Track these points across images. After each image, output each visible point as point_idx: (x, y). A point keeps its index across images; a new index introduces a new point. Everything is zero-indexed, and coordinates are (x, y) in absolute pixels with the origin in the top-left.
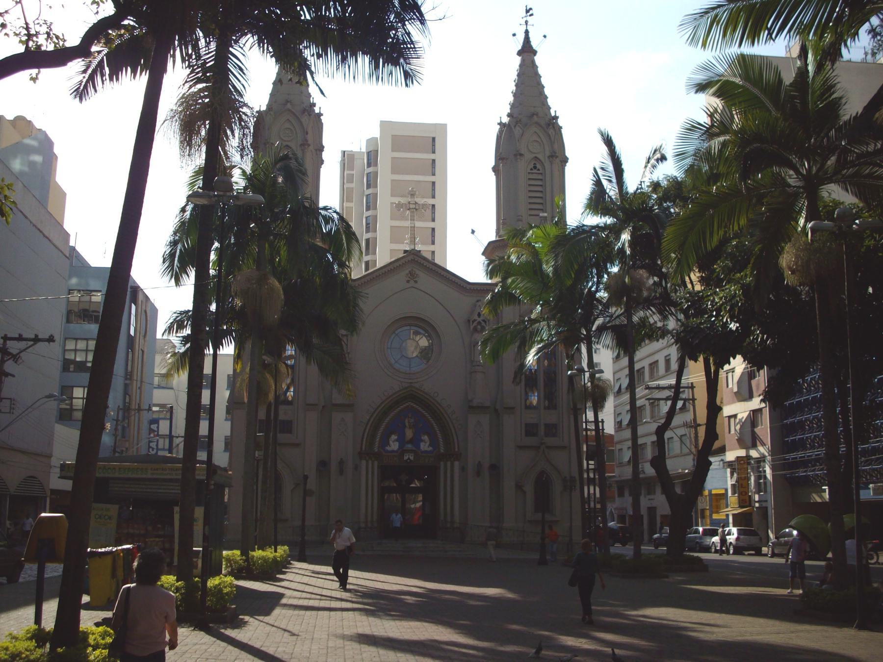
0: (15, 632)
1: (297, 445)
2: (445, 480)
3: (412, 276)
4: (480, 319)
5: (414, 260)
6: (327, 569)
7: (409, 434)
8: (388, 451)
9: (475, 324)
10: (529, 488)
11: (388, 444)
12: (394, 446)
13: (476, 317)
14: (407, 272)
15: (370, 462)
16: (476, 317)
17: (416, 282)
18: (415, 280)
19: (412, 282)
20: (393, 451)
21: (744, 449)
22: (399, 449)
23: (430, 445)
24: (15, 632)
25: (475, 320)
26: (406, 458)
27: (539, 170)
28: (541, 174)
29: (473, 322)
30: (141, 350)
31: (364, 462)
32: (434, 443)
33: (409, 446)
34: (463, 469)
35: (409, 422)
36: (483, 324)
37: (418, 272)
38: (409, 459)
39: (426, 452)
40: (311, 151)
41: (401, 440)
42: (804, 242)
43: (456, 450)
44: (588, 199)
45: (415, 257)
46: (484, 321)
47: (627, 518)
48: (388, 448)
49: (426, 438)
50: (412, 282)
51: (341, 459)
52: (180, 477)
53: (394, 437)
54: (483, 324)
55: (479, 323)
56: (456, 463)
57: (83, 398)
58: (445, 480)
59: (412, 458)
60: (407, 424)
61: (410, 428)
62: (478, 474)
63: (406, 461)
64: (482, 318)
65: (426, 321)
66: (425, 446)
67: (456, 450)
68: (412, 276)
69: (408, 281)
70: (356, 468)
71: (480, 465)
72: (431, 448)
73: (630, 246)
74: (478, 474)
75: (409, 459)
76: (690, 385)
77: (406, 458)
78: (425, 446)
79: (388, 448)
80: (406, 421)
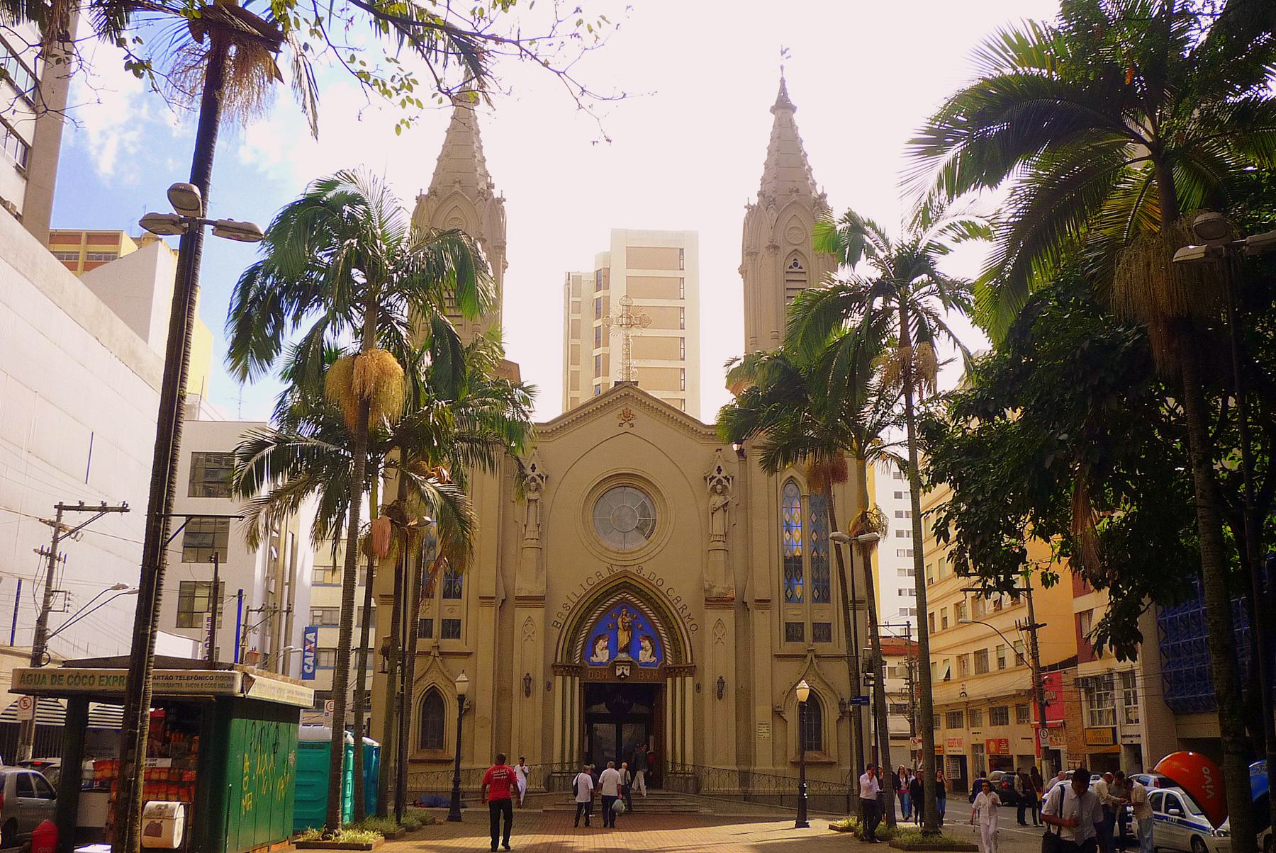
19: (626, 425)
50: (626, 425)
69: (621, 425)
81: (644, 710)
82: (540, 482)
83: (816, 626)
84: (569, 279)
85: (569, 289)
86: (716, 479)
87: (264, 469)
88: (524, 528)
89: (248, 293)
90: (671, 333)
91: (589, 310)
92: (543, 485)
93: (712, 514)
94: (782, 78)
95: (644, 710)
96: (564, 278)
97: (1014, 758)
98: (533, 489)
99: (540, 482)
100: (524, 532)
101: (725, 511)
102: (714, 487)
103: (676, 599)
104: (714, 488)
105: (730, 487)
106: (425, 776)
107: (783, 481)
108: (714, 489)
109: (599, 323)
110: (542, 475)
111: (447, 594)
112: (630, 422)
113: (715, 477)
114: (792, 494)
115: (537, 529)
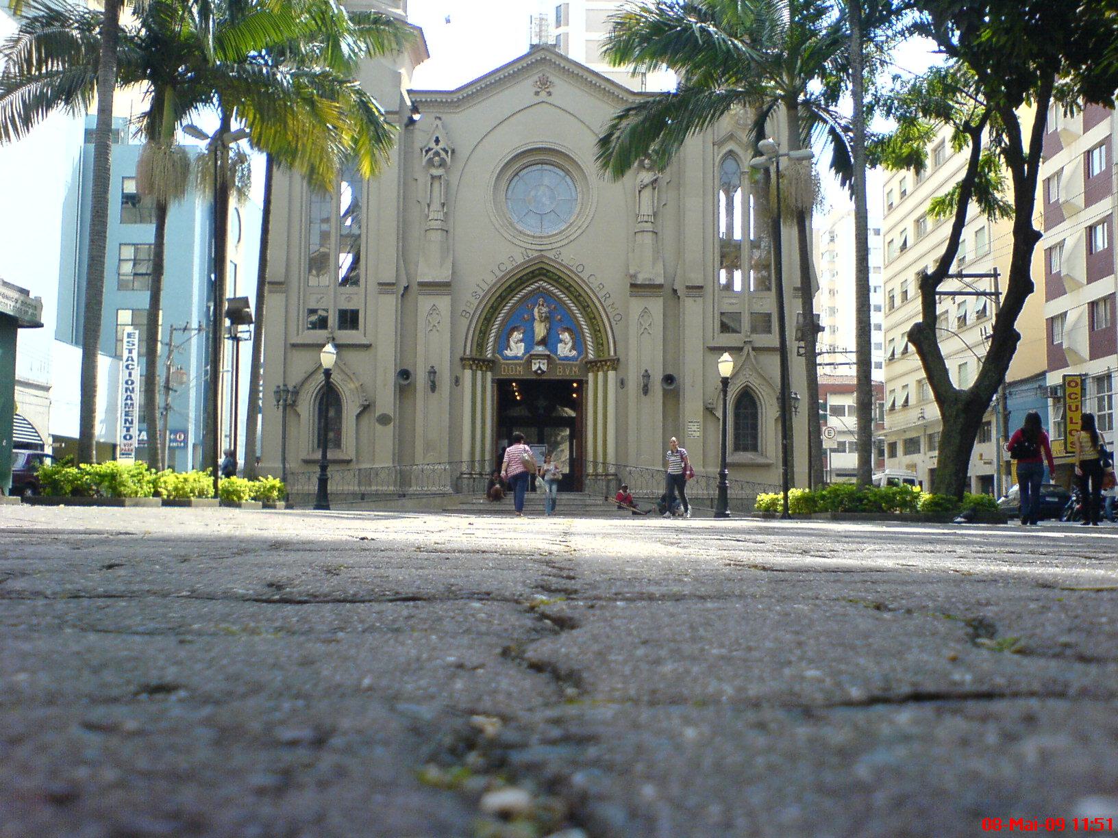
0: (474, 658)
1: (367, 347)
2: (483, 400)
3: (544, 84)
4: (438, 148)
5: (545, 59)
7: (540, 330)
8: (508, 358)
9: (431, 154)
10: (307, 407)
11: (508, 346)
12: (517, 348)
13: (432, 145)
14: (536, 78)
15: (479, 373)
16: (432, 145)
17: (549, 94)
18: (547, 90)
19: (543, 94)
20: (516, 358)
21: (16, 332)
22: (524, 354)
23: (573, 348)
24: (474, 658)
25: (430, 149)
26: (534, 368)
29: (427, 152)
31: (468, 373)
32: (578, 344)
33: (540, 349)
34: (622, 383)
35: (539, 312)
37: (552, 78)
38: (540, 368)
39: (566, 358)
41: (529, 341)
43: (612, 353)
45: (546, 53)
46: (444, 150)
47: (847, 446)
48: (508, 353)
49: (566, 336)
50: (543, 94)
51: (646, 371)
53: (517, 336)
55: (437, 154)
56: (611, 374)
57: (149, 260)
58: (483, 400)
59: (544, 368)
60: (537, 316)
61: (542, 322)
62: (646, 390)
63: (536, 372)
64: (442, 145)
65: (567, 156)
66: (565, 349)
67: (612, 353)
68: (544, 84)
69: (537, 93)
70: (457, 381)
71: (647, 376)
72: (574, 353)
73: (632, 55)
74: (646, 390)
75: (540, 368)
76: (992, 272)
77: (534, 368)
78: (565, 349)
79: (508, 353)
80: (536, 310)
81: (571, 413)
82: (445, 156)
92: (448, 160)
93: (640, 192)
99: (445, 156)
101: (654, 189)
107: (721, 155)
112: (547, 90)
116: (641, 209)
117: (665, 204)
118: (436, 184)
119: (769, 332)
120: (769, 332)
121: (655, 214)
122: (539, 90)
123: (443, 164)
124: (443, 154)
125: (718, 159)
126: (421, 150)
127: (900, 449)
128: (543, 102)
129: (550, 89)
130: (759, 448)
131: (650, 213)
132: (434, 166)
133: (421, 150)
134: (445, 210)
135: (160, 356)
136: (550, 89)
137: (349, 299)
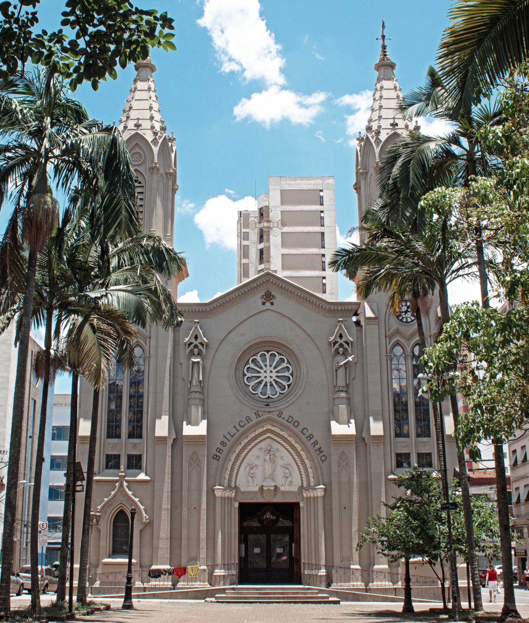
3: (268, 297)
4: (341, 341)
6: (355, 538)
9: (337, 345)
17: (272, 304)
18: (271, 301)
19: (268, 304)
27: (140, 183)
28: (143, 187)
29: (189, 345)
30: (32, 398)
36: (346, 345)
40: (50, 178)
42: (447, 348)
44: (197, 224)
46: (346, 342)
50: (268, 304)
52: (60, 541)
54: (346, 345)
55: (341, 345)
65: (285, 346)
68: (268, 297)
69: (264, 304)
81: (287, 523)
82: (202, 348)
83: (420, 456)
84: (241, 217)
85: (241, 223)
86: (338, 343)
87: (144, 447)
88: (189, 384)
89: (483, 620)
90: (315, 251)
91: (254, 236)
92: (204, 351)
93: (336, 370)
94: (383, 44)
95: (287, 523)
96: (236, 217)
97: (287, 188)
98: (196, 353)
99: (202, 348)
100: (189, 386)
101: (346, 368)
102: (337, 350)
103: (309, 436)
104: (337, 350)
105: (350, 350)
106: (114, 575)
107: (391, 343)
108: (337, 352)
109: (262, 246)
110: (203, 343)
111: (131, 436)
112: (271, 301)
113: (338, 342)
114: (398, 354)
115: (199, 385)
116: (338, 381)
117: (354, 378)
118: (196, 367)
119: (429, 436)
120: (429, 436)
121: (347, 385)
122: (265, 301)
123: (200, 354)
124: (200, 347)
125: (389, 347)
126: (186, 345)
127: (221, 447)
128: (268, 309)
129: (273, 301)
130: (433, 466)
131: (344, 384)
132: (194, 354)
133: (186, 345)
134: (202, 385)
135: (303, 508)
136: (273, 301)
137: (135, 446)
